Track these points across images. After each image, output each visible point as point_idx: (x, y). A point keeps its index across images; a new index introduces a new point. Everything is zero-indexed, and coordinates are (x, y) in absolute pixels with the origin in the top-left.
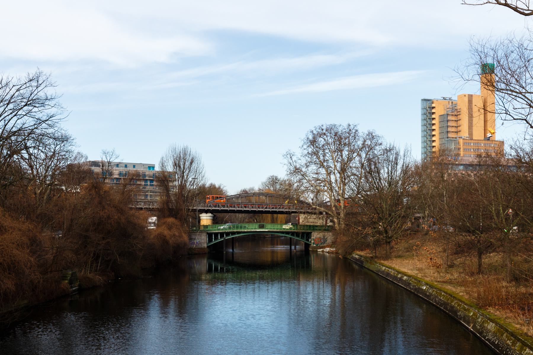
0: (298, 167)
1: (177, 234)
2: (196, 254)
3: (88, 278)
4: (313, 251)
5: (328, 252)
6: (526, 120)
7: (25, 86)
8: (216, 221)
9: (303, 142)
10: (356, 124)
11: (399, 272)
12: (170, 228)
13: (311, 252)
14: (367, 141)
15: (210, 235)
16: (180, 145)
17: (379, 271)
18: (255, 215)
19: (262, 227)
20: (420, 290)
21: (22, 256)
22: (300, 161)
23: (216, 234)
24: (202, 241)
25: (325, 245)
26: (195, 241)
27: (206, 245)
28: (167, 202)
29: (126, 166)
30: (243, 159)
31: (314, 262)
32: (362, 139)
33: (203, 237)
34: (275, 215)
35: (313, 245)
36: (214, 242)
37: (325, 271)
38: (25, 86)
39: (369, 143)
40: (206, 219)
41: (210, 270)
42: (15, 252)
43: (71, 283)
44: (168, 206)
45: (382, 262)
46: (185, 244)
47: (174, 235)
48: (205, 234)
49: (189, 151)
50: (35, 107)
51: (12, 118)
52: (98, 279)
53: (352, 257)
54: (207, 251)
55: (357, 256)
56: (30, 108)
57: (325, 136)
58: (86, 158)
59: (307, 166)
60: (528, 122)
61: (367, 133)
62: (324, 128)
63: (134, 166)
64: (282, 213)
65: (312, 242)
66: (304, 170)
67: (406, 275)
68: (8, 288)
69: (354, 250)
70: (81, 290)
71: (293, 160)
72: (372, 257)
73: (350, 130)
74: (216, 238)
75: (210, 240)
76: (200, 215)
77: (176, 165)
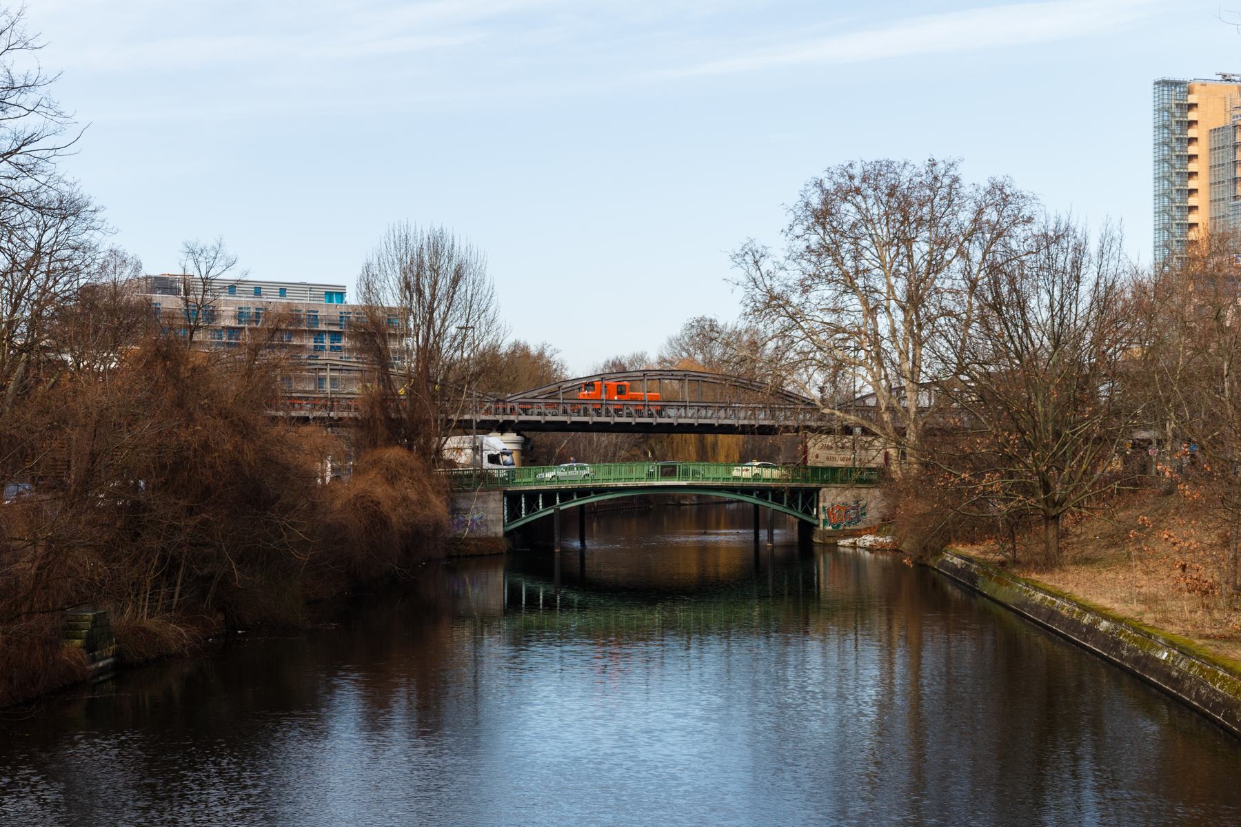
0: (778, 290)
1: (413, 495)
2: (472, 556)
3: (144, 630)
4: (824, 545)
5: (870, 549)
8: (531, 455)
9: (791, 216)
11: (1086, 609)
13: (817, 549)
15: (513, 499)
16: (422, 226)
17: (1025, 604)
18: (649, 436)
19: (669, 472)
20: (1149, 662)
23: (532, 497)
25: (861, 526)
26: (469, 517)
27: (499, 530)
28: (385, 400)
29: (258, 291)
31: (829, 580)
32: (971, 206)
33: (492, 505)
34: (710, 438)
36: (525, 518)
43: (91, 646)
44: (385, 409)
45: (1034, 576)
46: (438, 527)
48: (498, 496)
49: (448, 244)
52: (175, 633)
53: (944, 564)
54: (504, 546)
59: (806, 289)
61: (988, 186)
62: (857, 171)
63: (283, 292)
65: (822, 516)
66: (795, 299)
67: (1107, 618)
69: (949, 542)
70: (122, 669)
72: (1003, 564)
74: (531, 508)
75: (514, 514)
77: (410, 287)
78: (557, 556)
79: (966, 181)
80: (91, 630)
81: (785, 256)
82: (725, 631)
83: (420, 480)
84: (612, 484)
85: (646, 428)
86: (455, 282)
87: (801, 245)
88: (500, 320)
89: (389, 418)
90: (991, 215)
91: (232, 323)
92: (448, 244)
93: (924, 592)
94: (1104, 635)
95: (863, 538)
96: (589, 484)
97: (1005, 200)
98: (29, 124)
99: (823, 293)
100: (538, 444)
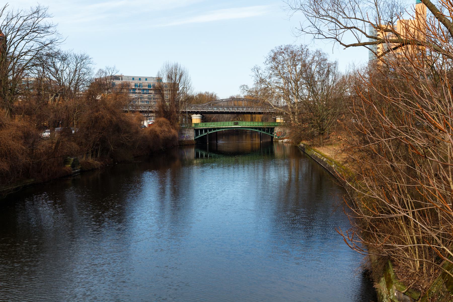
0: (263, 77)
1: (166, 130)
2: (186, 145)
3: (88, 163)
4: (275, 142)
5: (286, 143)
6: (336, 38)
7: (31, 17)
8: (204, 120)
9: (266, 59)
10: (307, 44)
11: (322, 156)
12: (161, 126)
13: (274, 143)
14: (315, 57)
15: (197, 131)
16: (172, 62)
17: (312, 155)
18: (238, 115)
19: (236, 124)
20: (331, 168)
21: (17, 145)
22: (264, 74)
23: (201, 130)
24: (190, 135)
25: (285, 137)
26: (185, 135)
27: (193, 139)
28: (163, 106)
29: (140, 79)
30: (223, 73)
31: (277, 151)
32: (311, 56)
33: (191, 132)
34: (254, 115)
35: (275, 137)
36: (200, 136)
37: (284, 157)
38: (31, 17)
39: (317, 59)
40: (196, 119)
41: (197, 156)
42: (11, 142)
43: (73, 166)
44: (163, 108)
45: (316, 148)
46: (174, 137)
47: (164, 131)
48: (193, 130)
49: (179, 67)
50: (39, 33)
51: (20, 42)
52: (97, 163)
53: (300, 146)
54: (194, 142)
55: (302, 145)
56: (35, 34)
57: (283, 54)
58: (106, 73)
59: (270, 77)
60: (337, 40)
61: (316, 51)
62: (283, 47)
63: (146, 79)
64: (260, 113)
65: (275, 135)
66: (268, 80)
67: (325, 158)
68: (3, 169)
69: (302, 140)
70: (82, 172)
71: (260, 73)
72: (310, 145)
73: (302, 49)
74: (201, 133)
75: (197, 134)
76: (192, 116)
77: (169, 77)
78: (208, 146)
79: (310, 49)
80: (73, 162)
81: (265, 70)
82: (243, 163)
83: (168, 126)
84: (222, 127)
85: (238, 113)
86: (181, 76)
87: (269, 66)
88: (192, 86)
89: (164, 111)
90: (316, 58)
91: (133, 87)
92: (179, 67)
93: (298, 153)
94: (324, 162)
95: (283, 139)
96: (216, 127)
97: (320, 54)
98: (53, 37)
99: (275, 79)
100: (205, 117)
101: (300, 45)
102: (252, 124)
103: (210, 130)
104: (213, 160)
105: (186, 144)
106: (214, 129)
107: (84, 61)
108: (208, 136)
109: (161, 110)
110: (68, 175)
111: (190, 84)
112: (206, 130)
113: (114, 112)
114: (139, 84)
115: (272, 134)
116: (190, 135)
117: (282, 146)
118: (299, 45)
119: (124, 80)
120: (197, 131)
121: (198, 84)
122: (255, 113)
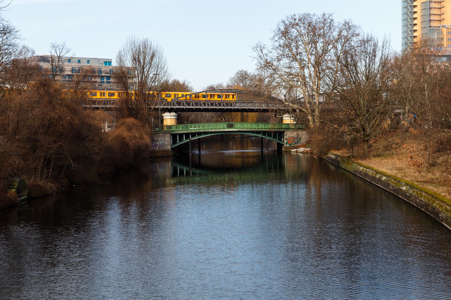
1: (137, 135)
2: (159, 157)
3: (38, 185)
4: (286, 151)
5: (303, 153)
8: (180, 120)
9: (274, 33)
11: (378, 172)
13: (284, 153)
15: (174, 136)
16: (140, 37)
17: (356, 171)
18: (224, 112)
19: (231, 126)
20: (399, 191)
23: (181, 135)
24: (166, 143)
26: (158, 143)
27: (169, 148)
29: (79, 61)
31: (289, 166)
33: (167, 138)
34: (245, 114)
36: (179, 143)
40: (169, 119)
41: (174, 174)
43: (19, 191)
45: (360, 161)
46: (147, 146)
47: (135, 137)
48: (169, 135)
52: (50, 186)
53: (328, 158)
54: (171, 153)
55: (333, 156)
59: (279, 60)
62: (297, 17)
65: (285, 141)
66: (275, 63)
67: (385, 176)
70: (30, 199)
72: (349, 157)
73: (325, 20)
74: (181, 140)
75: (174, 142)
76: (163, 115)
77: (136, 59)
79: (336, 21)
80: (18, 186)
83: (140, 130)
84: (210, 130)
86: (152, 58)
89: (128, 107)
90: (345, 33)
93: (322, 167)
94: (384, 181)
95: (299, 148)
96: (202, 131)
99: (285, 61)
101: (322, 14)
102: (266, 127)
103: (194, 134)
104: (186, 179)
105: (160, 155)
106: (200, 134)
107: (8, 35)
108: (190, 144)
109: (124, 105)
110: (11, 206)
111: (166, 68)
112: (187, 135)
113: (75, 110)
114: (77, 68)
115: (280, 140)
116: (166, 143)
117: (297, 158)
118: (320, 14)
119: (81, 64)
120: (174, 136)
121: (249, 72)
122: (245, 110)
